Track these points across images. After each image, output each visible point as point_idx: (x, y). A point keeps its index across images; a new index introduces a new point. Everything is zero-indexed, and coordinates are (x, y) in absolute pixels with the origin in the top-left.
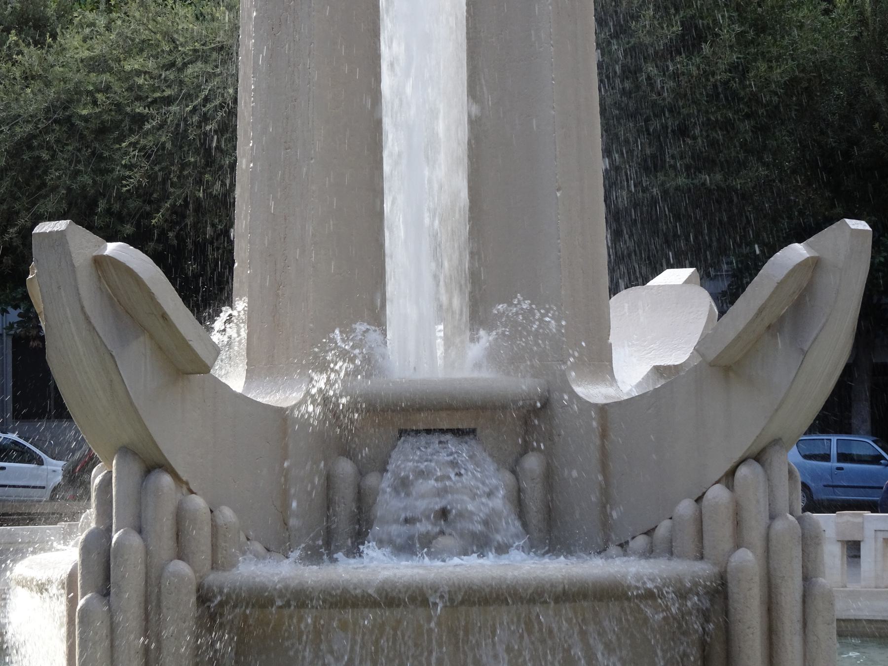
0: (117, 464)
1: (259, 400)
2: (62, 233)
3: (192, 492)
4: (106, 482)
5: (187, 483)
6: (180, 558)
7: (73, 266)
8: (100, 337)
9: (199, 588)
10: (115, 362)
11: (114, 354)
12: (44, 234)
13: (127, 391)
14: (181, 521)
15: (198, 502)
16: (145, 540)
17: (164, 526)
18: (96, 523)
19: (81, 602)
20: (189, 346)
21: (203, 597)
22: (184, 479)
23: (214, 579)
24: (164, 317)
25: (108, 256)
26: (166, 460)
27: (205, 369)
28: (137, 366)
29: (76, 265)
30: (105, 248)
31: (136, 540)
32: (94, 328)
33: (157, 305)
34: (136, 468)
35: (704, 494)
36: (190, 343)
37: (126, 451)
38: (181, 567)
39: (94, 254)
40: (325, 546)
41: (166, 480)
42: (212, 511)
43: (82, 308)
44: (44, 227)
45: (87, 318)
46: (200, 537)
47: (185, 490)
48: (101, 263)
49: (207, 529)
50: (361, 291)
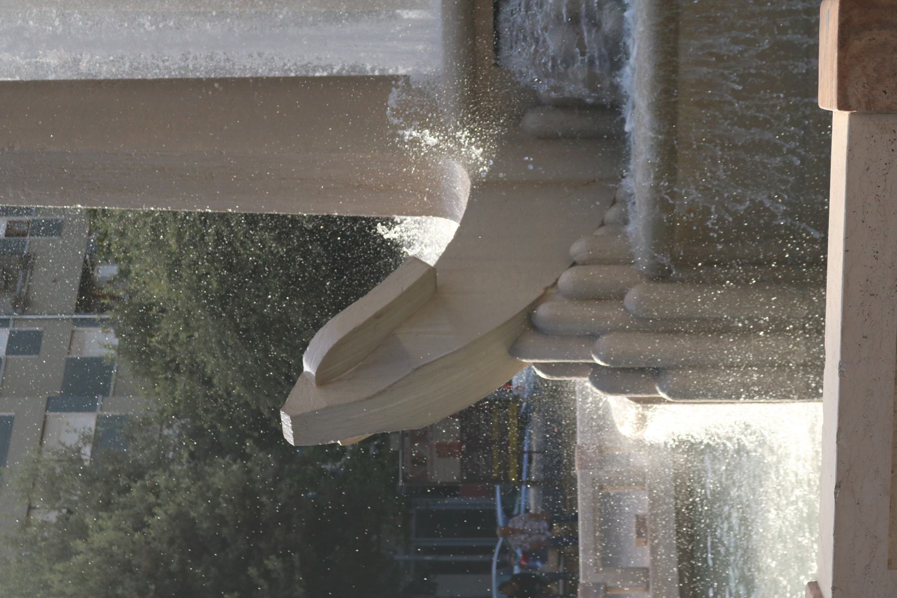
0: (527, 358)
1: (465, 208)
2: (294, 419)
3: (555, 284)
4: (544, 368)
5: (547, 289)
6: (622, 297)
7: (326, 408)
8: (399, 381)
9: (651, 279)
10: (424, 365)
11: (415, 367)
12: (294, 435)
13: (453, 353)
14: (587, 296)
15: (567, 278)
16: (605, 332)
17: (590, 313)
18: (584, 376)
19: (663, 395)
20: (409, 290)
21: (660, 275)
22: (542, 292)
23: (642, 262)
24: (378, 316)
25: (317, 373)
26: (522, 311)
27: (432, 272)
28: (427, 342)
29: (325, 405)
30: (308, 373)
31: (603, 340)
32: (390, 386)
33: (369, 320)
34: (532, 341)
35: (557, 280)
36: (404, 289)
37: (515, 350)
38: (632, 296)
39: (315, 385)
40: (615, 144)
41: (543, 311)
42: (574, 264)
43: (369, 398)
44: (289, 436)
45: (380, 393)
46: (600, 276)
47: (553, 291)
48: (324, 378)
49: (592, 271)
50: (356, 99)
